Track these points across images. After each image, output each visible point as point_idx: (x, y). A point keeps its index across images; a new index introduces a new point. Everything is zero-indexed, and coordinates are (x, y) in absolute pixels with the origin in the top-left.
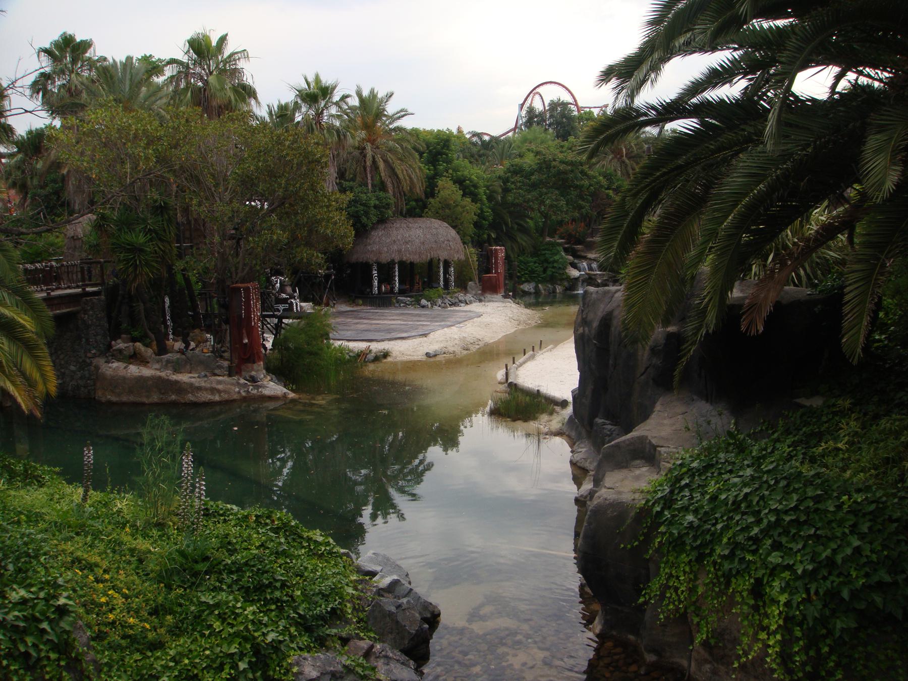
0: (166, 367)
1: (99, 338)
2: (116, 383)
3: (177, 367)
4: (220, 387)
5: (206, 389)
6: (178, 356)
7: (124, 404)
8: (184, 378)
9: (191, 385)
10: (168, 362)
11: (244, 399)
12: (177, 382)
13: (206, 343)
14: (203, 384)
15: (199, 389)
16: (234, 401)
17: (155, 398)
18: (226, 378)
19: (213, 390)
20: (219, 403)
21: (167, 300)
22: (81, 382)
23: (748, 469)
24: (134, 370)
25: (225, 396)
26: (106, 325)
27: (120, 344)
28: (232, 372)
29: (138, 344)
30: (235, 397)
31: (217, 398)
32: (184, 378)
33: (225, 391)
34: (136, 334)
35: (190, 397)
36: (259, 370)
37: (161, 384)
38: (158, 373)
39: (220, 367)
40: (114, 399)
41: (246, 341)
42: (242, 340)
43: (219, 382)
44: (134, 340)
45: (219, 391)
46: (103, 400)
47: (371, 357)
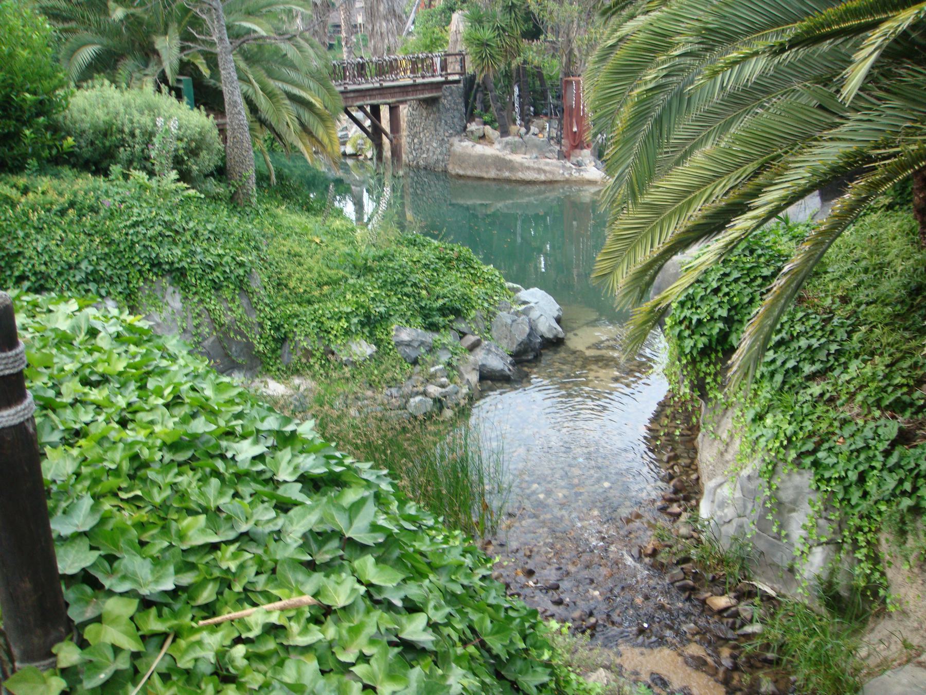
0: (505, 147)
1: (456, 120)
2: (462, 159)
3: (514, 149)
4: (547, 168)
5: (534, 169)
6: (517, 139)
7: (469, 177)
8: (517, 158)
9: (522, 164)
10: (507, 143)
11: (567, 181)
12: (511, 161)
13: (544, 129)
14: (532, 165)
15: (528, 168)
16: (556, 182)
17: (492, 174)
18: (554, 161)
19: (539, 170)
20: (544, 182)
21: (516, 89)
22: (440, 157)
23: (64, 325)
24: (481, 149)
25: (550, 177)
26: (464, 110)
27: (472, 127)
28: (563, 156)
29: (488, 128)
30: (559, 178)
31: (542, 177)
32: (517, 158)
33: (550, 172)
34: (486, 118)
35: (520, 175)
36: (586, 155)
37: (500, 163)
38: (498, 153)
39: (551, 151)
40: (461, 172)
41: (575, 129)
42: (572, 127)
43: (547, 164)
44: (485, 123)
45: (545, 172)
46: (453, 172)
47: (253, 35)
